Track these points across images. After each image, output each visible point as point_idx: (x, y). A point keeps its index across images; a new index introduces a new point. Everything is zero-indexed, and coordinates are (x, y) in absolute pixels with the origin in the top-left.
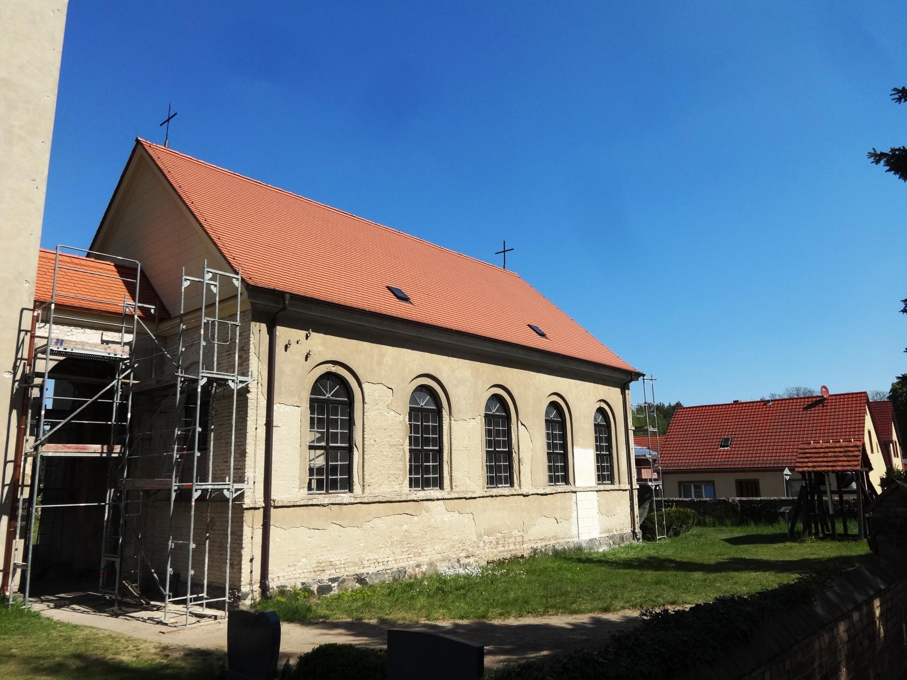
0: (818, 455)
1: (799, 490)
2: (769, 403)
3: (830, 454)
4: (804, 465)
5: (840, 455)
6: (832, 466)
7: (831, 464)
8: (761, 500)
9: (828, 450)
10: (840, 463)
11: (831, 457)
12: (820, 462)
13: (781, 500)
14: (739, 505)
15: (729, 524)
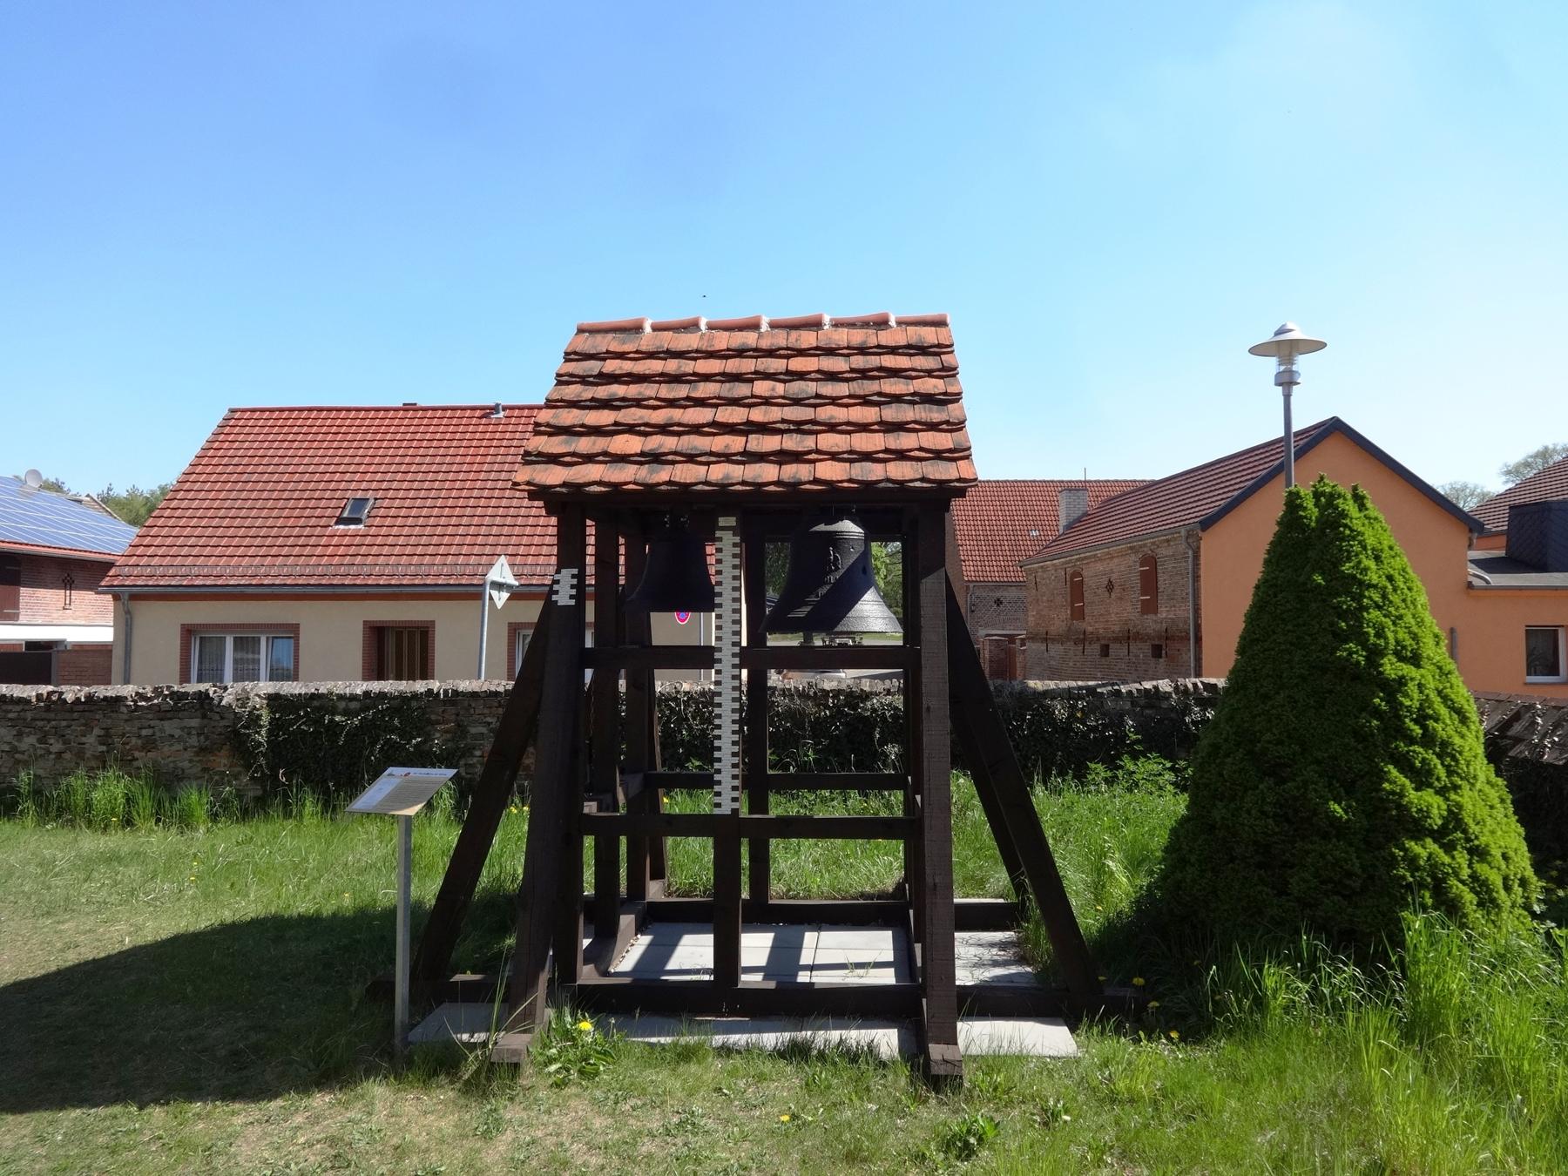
0: (681, 391)
1: (536, 621)
2: (498, 412)
3: (762, 388)
4: (585, 445)
5: (829, 389)
6: (783, 457)
7: (770, 443)
8: (367, 694)
9: (747, 365)
10: (829, 441)
11: (767, 401)
12: (696, 429)
13: (456, 693)
14: (265, 719)
15: (201, 812)
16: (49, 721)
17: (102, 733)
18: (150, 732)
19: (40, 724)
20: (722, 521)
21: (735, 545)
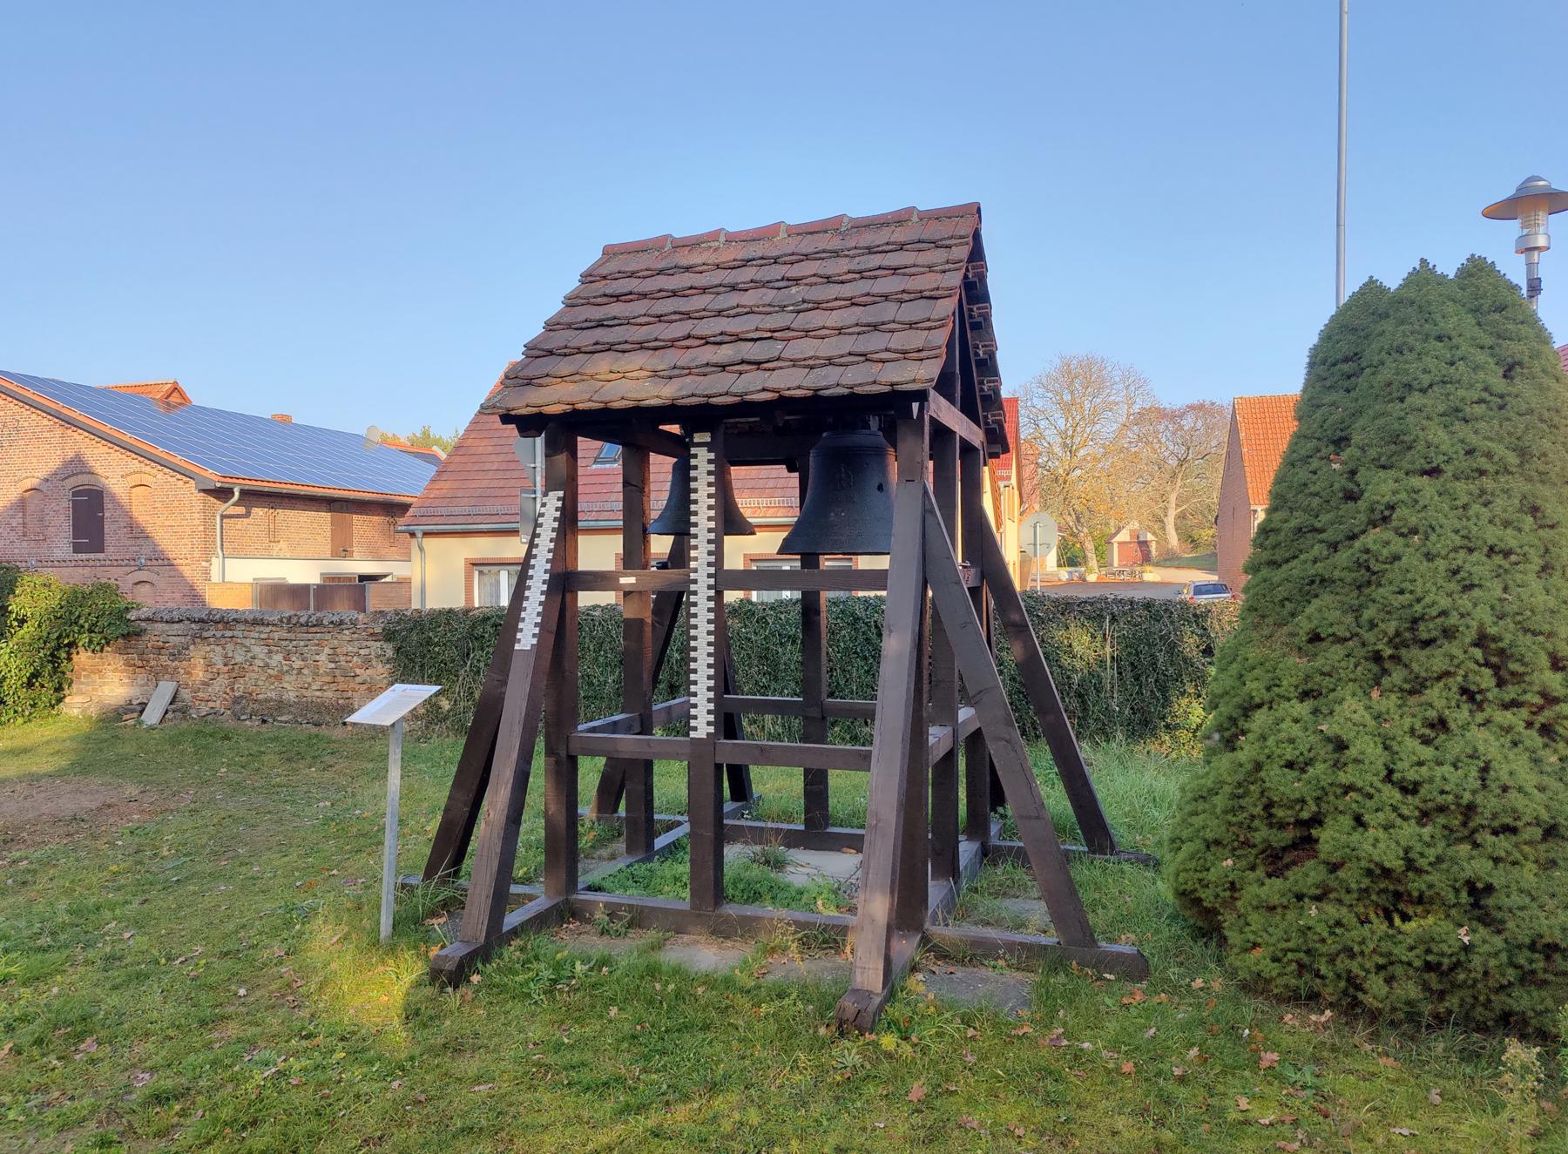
16: (291, 640)
17: (331, 652)
19: (285, 643)
20: (698, 438)
21: (710, 462)
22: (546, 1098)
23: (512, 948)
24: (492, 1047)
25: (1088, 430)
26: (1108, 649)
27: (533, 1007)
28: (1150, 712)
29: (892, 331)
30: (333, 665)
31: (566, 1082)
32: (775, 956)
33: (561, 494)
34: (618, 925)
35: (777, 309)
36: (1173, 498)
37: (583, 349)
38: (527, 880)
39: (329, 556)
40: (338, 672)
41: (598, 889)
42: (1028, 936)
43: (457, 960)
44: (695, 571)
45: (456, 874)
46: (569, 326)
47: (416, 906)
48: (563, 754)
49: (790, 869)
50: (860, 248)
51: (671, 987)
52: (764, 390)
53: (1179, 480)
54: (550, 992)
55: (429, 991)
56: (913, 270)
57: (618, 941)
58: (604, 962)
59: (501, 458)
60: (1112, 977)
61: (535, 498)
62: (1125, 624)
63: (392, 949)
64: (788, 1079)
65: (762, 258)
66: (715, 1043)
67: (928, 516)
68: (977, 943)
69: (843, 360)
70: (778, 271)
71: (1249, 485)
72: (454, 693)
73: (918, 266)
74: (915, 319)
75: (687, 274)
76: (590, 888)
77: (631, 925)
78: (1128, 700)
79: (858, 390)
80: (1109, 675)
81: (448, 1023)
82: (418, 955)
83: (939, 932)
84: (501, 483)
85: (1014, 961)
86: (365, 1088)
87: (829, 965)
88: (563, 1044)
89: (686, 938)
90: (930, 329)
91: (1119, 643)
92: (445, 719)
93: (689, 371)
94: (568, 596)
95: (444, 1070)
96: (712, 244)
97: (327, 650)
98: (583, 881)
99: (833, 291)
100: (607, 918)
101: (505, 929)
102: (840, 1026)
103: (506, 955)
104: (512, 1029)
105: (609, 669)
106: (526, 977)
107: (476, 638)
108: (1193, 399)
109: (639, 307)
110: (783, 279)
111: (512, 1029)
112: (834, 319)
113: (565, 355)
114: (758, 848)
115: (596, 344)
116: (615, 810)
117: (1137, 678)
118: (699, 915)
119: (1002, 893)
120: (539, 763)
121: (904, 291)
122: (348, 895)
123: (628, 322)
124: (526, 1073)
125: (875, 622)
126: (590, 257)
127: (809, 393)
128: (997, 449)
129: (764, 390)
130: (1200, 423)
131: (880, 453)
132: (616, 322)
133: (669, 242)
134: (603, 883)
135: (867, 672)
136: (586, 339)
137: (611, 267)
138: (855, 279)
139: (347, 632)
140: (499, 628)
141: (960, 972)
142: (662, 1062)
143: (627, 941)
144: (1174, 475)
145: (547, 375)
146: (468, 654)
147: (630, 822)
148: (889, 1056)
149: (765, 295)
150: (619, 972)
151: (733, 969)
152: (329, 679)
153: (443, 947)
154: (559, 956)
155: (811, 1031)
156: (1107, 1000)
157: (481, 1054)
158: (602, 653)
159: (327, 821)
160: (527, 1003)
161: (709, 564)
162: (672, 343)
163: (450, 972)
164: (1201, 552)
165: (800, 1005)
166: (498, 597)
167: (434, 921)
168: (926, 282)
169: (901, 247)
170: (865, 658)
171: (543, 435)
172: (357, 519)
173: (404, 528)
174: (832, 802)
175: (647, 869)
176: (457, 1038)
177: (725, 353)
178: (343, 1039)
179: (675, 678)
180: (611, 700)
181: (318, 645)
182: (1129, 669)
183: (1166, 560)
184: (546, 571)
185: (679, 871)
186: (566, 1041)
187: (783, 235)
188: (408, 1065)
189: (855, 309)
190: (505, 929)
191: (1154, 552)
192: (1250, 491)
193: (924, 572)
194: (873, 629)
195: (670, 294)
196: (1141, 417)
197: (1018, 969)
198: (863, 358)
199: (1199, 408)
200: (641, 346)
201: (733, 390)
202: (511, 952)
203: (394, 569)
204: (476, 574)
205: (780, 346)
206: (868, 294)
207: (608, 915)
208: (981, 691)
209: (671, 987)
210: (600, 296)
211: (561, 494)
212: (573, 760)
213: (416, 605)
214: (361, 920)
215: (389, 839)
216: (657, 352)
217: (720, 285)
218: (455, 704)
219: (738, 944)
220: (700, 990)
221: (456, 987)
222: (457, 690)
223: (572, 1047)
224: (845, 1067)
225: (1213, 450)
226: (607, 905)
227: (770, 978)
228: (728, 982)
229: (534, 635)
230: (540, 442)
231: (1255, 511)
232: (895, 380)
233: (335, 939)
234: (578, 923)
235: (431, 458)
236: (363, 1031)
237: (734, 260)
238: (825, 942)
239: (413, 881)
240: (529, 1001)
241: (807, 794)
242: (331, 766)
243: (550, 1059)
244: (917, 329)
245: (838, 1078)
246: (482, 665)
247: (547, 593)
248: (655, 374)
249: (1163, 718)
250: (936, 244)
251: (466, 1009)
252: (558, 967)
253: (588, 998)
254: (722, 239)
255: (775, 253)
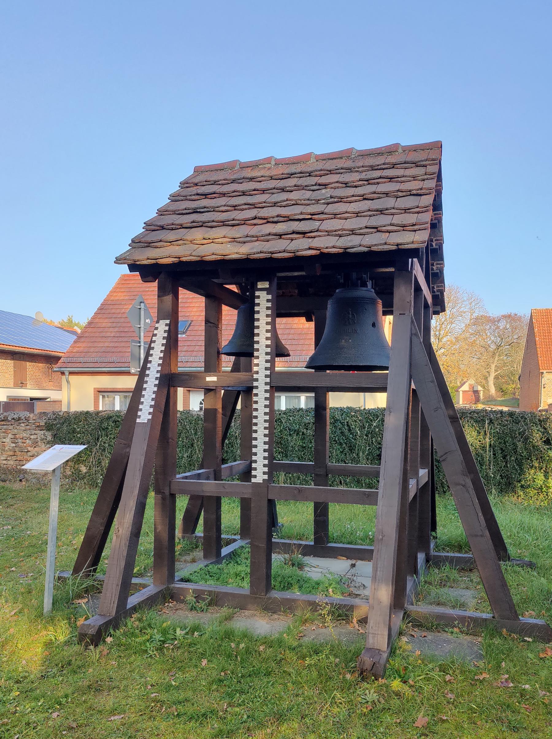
17: (13, 437)
18: (35, 437)
20: (260, 285)
21: (268, 301)
22: (163, 726)
23: (133, 619)
24: (122, 688)
25: (449, 327)
26: (487, 440)
27: (149, 659)
28: (512, 477)
29: (393, 214)
30: (14, 445)
31: (176, 713)
32: (307, 625)
33: (168, 322)
34: (202, 604)
35: (313, 202)
36: (493, 367)
37: (184, 226)
38: (140, 575)
39: (12, 386)
40: (17, 449)
41: (187, 580)
42: (470, 613)
43: (97, 628)
44: (257, 373)
45: (95, 570)
46: (174, 212)
47: (68, 592)
48: (167, 493)
49: (306, 569)
50: (366, 167)
51: (242, 645)
52: (310, 249)
53: (497, 357)
54: (160, 649)
55: (77, 648)
56: (403, 179)
57: (201, 615)
58: (196, 628)
59: (116, 330)
60: (530, 640)
61: (140, 346)
62: (498, 425)
63: (51, 620)
64: (329, 711)
65: (301, 173)
66: (277, 685)
67: (414, 338)
68: (440, 616)
69: (362, 231)
70: (313, 181)
71: (540, 359)
72: (89, 462)
73: (406, 176)
74: (408, 206)
75: (251, 183)
76: (182, 580)
77: (210, 604)
78: (499, 470)
79: (374, 249)
80: (488, 455)
81: (91, 670)
82: (70, 623)
83: (415, 609)
84: (117, 344)
85: (465, 629)
86: (33, 718)
87: (343, 631)
88: (172, 685)
89: (247, 613)
90: (418, 212)
91: (494, 437)
92: (83, 478)
93: (257, 238)
94: (172, 389)
95: (89, 705)
96: (267, 166)
97: (10, 436)
98: (178, 575)
99: (350, 191)
100: (194, 600)
101: (129, 606)
102: (362, 673)
103: (129, 624)
104: (136, 675)
105: (185, 449)
106: (144, 639)
107: (103, 429)
108: (505, 312)
109: (222, 201)
110: (316, 185)
111: (136, 675)
112: (353, 207)
113: (172, 229)
114: (287, 556)
115: (194, 222)
116: (193, 531)
117: (504, 457)
118: (256, 598)
119: (442, 584)
120: (152, 498)
121: (398, 191)
122: (22, 583)
123: (214, 210)
124: (147, 707)
125: (347, 422)
126: (187, 173)
127: (341, 251)
128: (438, 308)
129: (310, 249)
130: (508, 326)
131: (373, 302)
132: (205, 210)
133: (238, 164)
134: (191, 577)
135: (342, 452)
136: (186, 220)
137: (201, 178)
138: (364, 185)
139: (22, 425)
140: (117, 423)
141: (430, 636)
142: (242, 699)
143: (209, 615)
144: (494, 354)
145: (161, 241)
146: (98, 439)
147: (207, 538)
148: (398, 694)
149: (304, 194)
150: (207, 635)
151: (281, 634)
152: (11, 453)
153: (86, 619)
154: (165, 625)
155: (341, 677)
156: (529, 655)
157: (114, 693)
158: (181, 439)
159: (9, 537)
160: (145, 657)
161: (266, 369)
162: (244, 222)
163: (93, 635)
164: (507, 397)
165: (332, 658)
166: (114, 404)
167: (80, 601)
168: (414, 185)
169: (393, 166)
170: (341, 444)
171: (157, 280)
172: (29, 365)
173: (57, 369)
174: (330, 528)
175: (218, 568)
176: (97, 681)
177: (281, 228)
178: (18, 682)
179: (225, 455)
180: (186, 467)
181: (4, 432)
182: (500, 452)
183: (488, 401)
184: (158, 372)
185: (239, 570)
186: (174, 683)
187: (313, 160)
188: (64, 701)
189: (366, 201)
190: (129, 606)
191: (482, 397)
192: (540, 362)
193: (410, 371)
194: (346, 427)
195: (240, 194)
196: (478, 321)
197: (467, 634)
198: (375, 230)
199: (508, 317)
200: (224, 224)
201: (289, 248)
202: (132, 622)
203: (52, 395)
204: (101, 397)
205: (318, 223)
206: (375, 193)
207: (195, 597)
208: (446, 453)
209: (242, 645)
210: (194, 195)
211: (168, 322)
212: (173, 497)
213: (64, 409)
214: (31, 600)
215: (50, 548)
216: (234, 228)
217: (274, 188)
218: (90, 469)
219: (281, 617)
220: (261, 648)
221: (96, 645)
222: (91, 460)
223: (177, 688)
224: (367, 702)
225: (515, 341)
226: (194, 591)
227: (306, 639)
228: (280, 642)
229: (150, 413)
230: (154, 285)
231: (542, 373)
232: (400, 241)
233: (13, 613)
234: (175, 602)
235: (74, 333)
236: (32, 676)
237: (282, 174)
238: (339, 616)
239: (65, 575)
240: (146, 655)
241: (316, 522)
242: (12, 505)
243: (163, 697)
244: (410, 213)
245: (365, 710)
246: (107, 445)
247: (159, 386)
248: (234, 240)
249: (520, 481)
250: (417, 164)
251: (103, 661)
252: (164, 632)
253: (186, 654)
254: (273, 163)
255: (309, 169)
